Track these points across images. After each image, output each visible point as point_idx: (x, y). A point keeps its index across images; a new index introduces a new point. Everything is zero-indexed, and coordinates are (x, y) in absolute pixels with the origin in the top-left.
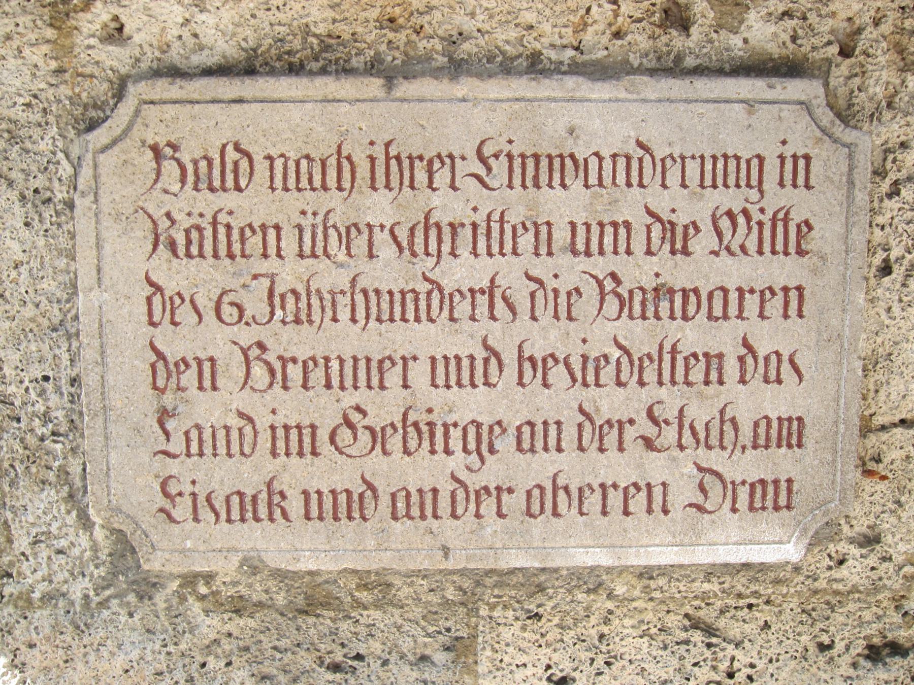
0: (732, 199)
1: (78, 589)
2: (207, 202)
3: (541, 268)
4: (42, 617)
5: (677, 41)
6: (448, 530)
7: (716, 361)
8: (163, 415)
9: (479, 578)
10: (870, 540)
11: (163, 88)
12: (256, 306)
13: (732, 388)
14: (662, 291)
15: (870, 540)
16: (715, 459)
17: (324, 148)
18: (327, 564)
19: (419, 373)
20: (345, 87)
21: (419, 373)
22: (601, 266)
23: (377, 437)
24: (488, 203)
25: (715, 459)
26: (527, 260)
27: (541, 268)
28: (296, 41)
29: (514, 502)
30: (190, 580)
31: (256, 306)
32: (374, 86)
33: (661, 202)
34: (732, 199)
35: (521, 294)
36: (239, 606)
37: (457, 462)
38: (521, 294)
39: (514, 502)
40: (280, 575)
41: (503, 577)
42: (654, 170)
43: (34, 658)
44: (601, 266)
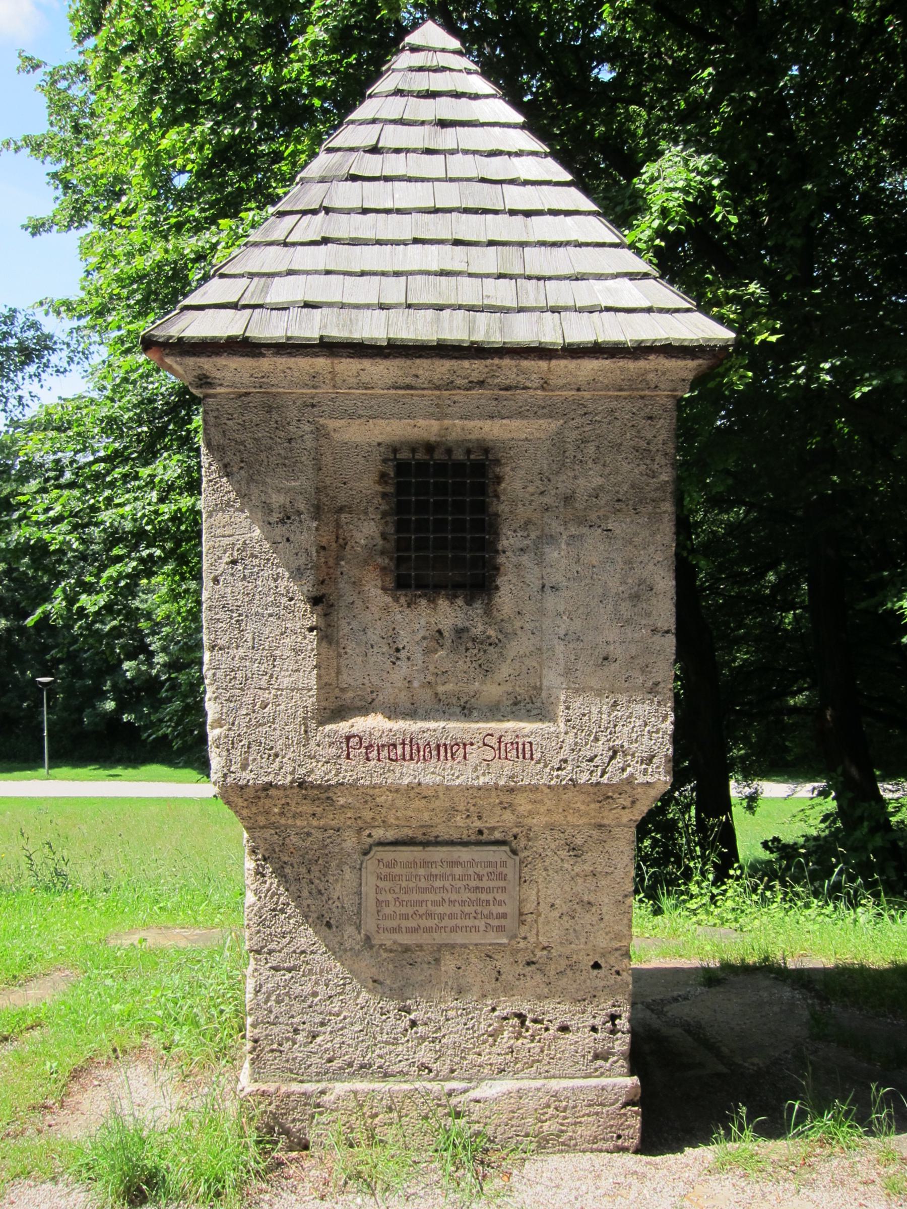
0: (490, 870)
1: (357, 947)
2: (388, 870)
3: (453, 883)
4: (349, 954)
5: (480, 837)
6: (435, 935)
7: (488, 902)
8: (378, 912)
9: (441, 945)
10: (525, 938)
11: (380, 848)
12: (397, 890)
13: (492, 907)
14: (477, 888)
15: (525, 938)
16: (489, 921)
17: (411, 859)
18: (409, 942)
19: (429, 904)
20: (415, 849)
21: (429, 904)
22: (465, 883)
23: (421, 916)
24: (443, 871)
25: (489, 921)
26: (450, 882)
27: (453, 883)
28: (89, 487)
29: (448, 930)
30: (381, 945)
31: (397, 890)
32: (421, 848)
33: (477, 870)
34: (490, 870)
35: (449, 888)
36: (391, 951)
37: (436, 921)
38: (449, 888)
39: (448, 930)
40: (401, 944)
41: (446, 945)
42: (444, 69)
43: (347, 963)
44: (465, 883)
